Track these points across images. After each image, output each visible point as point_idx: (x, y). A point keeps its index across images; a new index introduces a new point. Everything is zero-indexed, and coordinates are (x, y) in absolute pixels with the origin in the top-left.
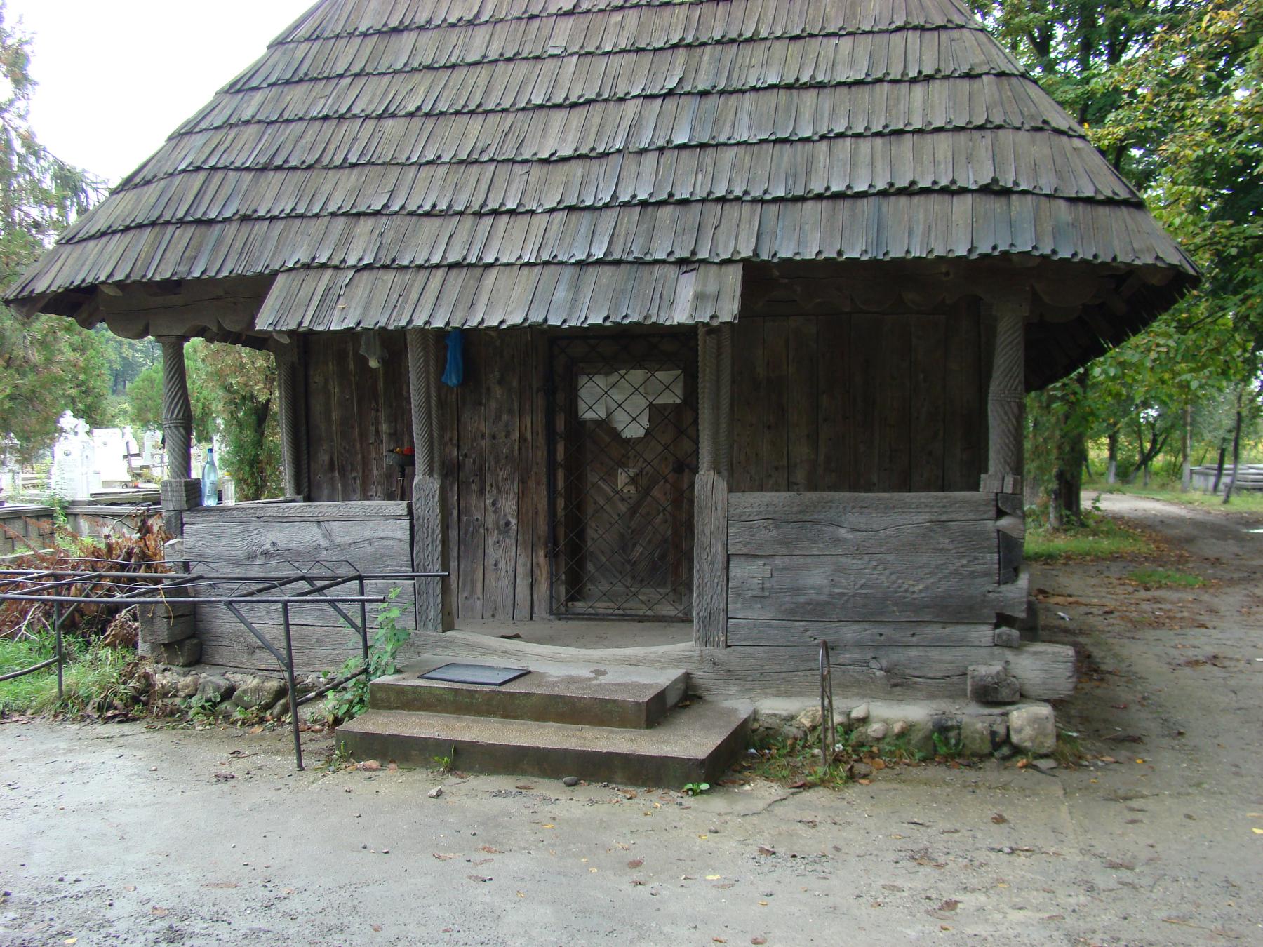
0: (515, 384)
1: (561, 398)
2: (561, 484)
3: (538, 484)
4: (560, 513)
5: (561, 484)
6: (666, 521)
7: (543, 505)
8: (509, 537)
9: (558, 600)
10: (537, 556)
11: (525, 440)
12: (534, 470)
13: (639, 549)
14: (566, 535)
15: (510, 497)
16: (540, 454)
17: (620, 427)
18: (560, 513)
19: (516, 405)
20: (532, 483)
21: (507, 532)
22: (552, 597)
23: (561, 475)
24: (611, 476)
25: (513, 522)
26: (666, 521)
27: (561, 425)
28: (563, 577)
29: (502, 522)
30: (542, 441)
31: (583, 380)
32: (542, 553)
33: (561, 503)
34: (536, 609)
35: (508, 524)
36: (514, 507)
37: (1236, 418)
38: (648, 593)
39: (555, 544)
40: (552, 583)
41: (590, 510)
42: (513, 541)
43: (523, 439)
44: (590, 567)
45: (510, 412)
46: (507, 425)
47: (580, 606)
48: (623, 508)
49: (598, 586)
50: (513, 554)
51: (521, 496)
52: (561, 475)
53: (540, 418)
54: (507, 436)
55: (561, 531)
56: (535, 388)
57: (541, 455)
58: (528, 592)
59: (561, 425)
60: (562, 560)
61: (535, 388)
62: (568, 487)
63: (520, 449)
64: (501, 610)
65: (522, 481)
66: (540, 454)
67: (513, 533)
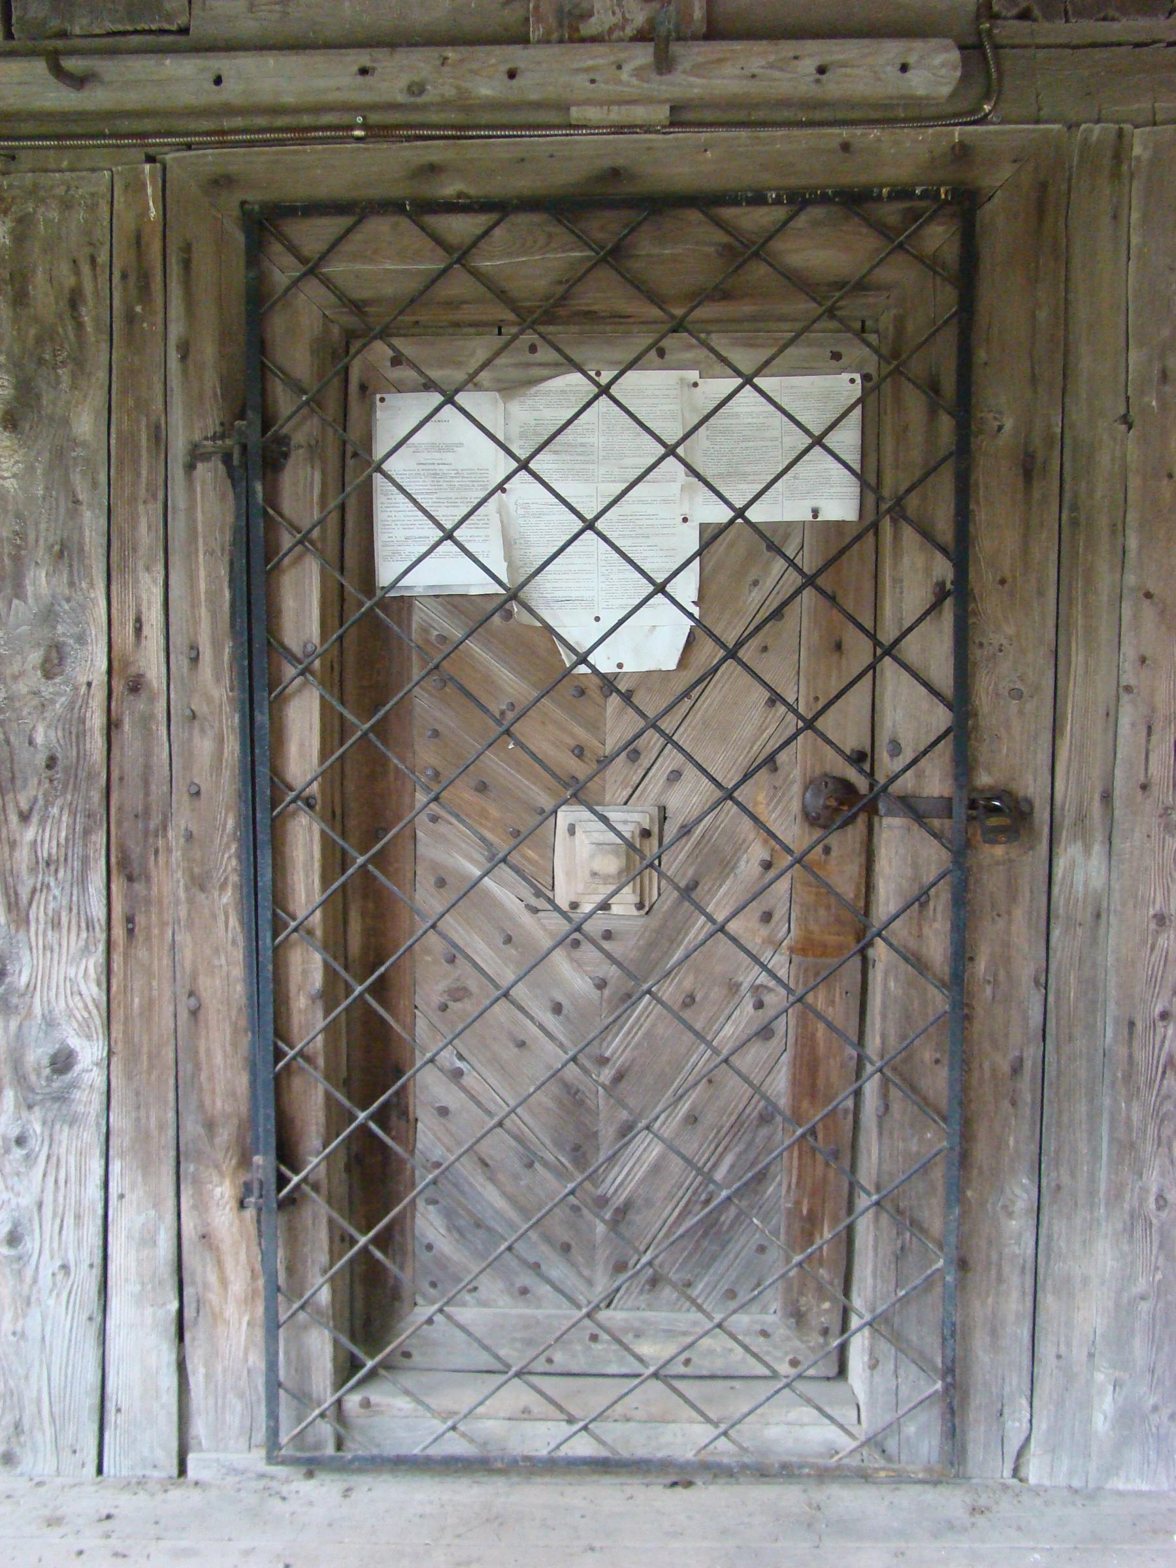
0: (85, 424)
1: (301, 491)
2: (306, 888)
3: (199, 882)
4: (309, 1021)
5: (306, 888)
6: (765, 1032)
7: (225, 979)
8: (73, 1121)
9: (303, 1398)
10: (201, 1206)
11: (136, 686)
12: (183, 819)
13: (646, 1151)
14: (336, 1117)
15: (73, 941)
16: (204, 746)
17: (577, 629)
18: (309, 1021)
19: (92, 524)
20: (169, 879)
21: (62, 1098)
22: (273, 1385)
23: (305, 840)
24: (521, 846)
25: (89, 1053)
26: (765, 1032)
27: (302, 612)
28: (324, 1296)
29: (37, 1055)
30: (214, 687)
31: (396, 416)
32: (223, 1191)
33: (307, 968)
34: (200, 1427)
35: (63, 1062)
36: (93, 991)
37: (655, 812)
38: (659, 1329)
39: (287, 1153)
40: (272, 1326)
41: (430, 985)
42: (91, 1137)
43: (123, 680)
44: (429, 1225)
45: (65, 553)
46: (49, 616)
47: (396, 1414)
48: (573, 976)
49: (466, 1313)
50: (94, 1192)
51: (123, 934)
52: (305, 840)
53: (207, 580)
54: (54, 663)
55: (312, 1099)
56: (179, 446)
57: (211, 752)
58: (168, 1356)
59: (302, 612)
60: (318, 1216)
61: (179, 446)
62: (337, 907)
63: (112, 726)
64: (44, 1437)
65: (125, 868)
66: (204, 746)
67: (88, 1101)
